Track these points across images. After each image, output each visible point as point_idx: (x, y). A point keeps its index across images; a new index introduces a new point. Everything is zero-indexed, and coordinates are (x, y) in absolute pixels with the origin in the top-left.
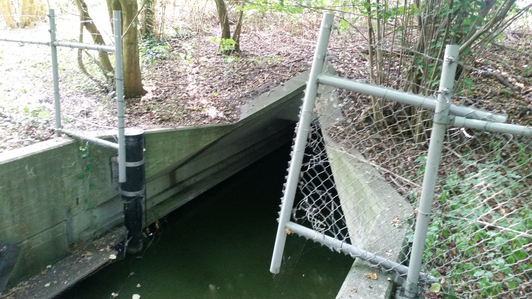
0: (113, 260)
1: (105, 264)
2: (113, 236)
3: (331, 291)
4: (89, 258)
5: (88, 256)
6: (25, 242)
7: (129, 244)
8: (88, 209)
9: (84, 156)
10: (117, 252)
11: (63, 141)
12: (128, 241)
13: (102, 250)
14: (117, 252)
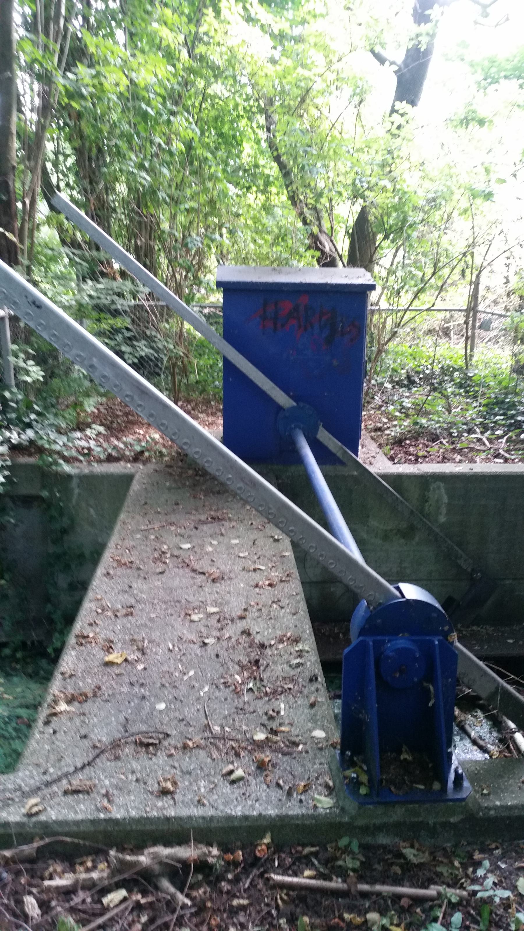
6: (507, 582)
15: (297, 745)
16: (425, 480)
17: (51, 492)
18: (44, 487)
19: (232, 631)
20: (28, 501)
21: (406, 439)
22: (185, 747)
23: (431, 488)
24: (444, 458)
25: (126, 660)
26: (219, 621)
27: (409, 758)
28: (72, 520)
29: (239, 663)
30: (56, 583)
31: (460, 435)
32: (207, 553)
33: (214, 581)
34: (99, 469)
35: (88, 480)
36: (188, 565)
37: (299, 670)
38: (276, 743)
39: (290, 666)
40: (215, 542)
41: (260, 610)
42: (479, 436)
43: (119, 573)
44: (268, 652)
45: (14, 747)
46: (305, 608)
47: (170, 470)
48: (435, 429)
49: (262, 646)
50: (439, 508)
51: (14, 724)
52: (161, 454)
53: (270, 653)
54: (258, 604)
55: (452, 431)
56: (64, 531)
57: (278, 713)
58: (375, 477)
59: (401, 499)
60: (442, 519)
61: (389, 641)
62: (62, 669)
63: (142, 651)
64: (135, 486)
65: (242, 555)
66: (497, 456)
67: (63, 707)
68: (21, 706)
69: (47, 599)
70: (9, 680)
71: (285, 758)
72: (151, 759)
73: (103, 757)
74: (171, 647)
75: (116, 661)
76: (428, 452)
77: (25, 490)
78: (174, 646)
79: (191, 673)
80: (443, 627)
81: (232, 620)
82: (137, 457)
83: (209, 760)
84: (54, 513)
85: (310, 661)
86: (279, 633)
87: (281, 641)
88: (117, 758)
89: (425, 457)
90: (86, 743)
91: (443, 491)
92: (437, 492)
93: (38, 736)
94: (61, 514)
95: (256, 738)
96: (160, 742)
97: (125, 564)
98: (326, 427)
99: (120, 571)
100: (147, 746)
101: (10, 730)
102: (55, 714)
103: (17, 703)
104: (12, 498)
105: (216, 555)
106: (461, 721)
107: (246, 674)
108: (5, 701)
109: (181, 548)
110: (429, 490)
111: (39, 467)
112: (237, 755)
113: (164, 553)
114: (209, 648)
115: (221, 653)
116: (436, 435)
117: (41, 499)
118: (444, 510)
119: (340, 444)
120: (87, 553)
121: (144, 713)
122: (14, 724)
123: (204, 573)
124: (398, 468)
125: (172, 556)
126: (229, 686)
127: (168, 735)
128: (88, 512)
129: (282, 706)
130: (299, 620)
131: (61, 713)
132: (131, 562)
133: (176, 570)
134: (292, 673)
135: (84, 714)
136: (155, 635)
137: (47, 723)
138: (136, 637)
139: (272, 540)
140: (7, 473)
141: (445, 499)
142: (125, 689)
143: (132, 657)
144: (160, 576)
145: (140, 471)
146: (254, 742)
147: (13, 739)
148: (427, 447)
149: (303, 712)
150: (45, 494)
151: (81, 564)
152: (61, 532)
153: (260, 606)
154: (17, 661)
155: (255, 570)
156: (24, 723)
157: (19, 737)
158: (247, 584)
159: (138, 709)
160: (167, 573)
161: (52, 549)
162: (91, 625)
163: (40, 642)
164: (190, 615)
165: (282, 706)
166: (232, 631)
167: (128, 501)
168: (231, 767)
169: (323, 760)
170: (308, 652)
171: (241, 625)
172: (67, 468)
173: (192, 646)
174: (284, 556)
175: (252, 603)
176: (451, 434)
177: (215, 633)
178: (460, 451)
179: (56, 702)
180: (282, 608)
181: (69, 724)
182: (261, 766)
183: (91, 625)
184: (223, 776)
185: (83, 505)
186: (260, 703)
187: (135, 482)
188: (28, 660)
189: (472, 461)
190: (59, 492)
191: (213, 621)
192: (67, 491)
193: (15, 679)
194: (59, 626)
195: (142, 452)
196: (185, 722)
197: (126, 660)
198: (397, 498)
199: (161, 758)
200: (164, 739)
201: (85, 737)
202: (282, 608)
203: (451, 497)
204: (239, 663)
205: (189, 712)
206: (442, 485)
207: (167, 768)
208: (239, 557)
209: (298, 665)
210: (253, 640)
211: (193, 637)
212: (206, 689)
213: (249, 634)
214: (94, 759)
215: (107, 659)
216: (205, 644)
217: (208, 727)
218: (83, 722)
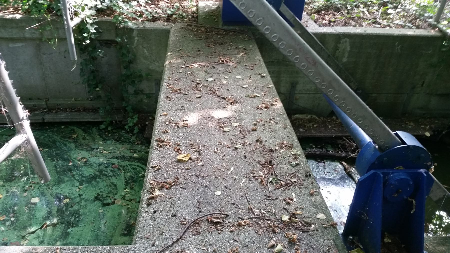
0: (427, 137)
1: (108, 41)
2: (437, 121)
3: (357, 238)
4: (410, 127)
5: (410, 125)
6: (374, 95)
7: (446, 133)
8: (427, 94)
9: (444, 49)
10: (433, 133)
11: (432, 32)
12: (446, 131)
13: (423, 126)
14: (433, 133)
15: (310, 225)
16: (339, 37)
17: (122, 38)
18: (117, 36)
19: (250, 139)
20: (108, 43)
21: (322, 10)
22: (240, 225)
23: (342, 42)
24: (346, 23)
25: (190, 159)
26: (241, 132)
27: (389, 241)
28: (135, 56)
29: (259, 162)
30: (127, 91)
31: (352, 9)
32: (223, 85)
33: (231, 103)
34: (149, 25)
35: (143, 32)
36: (214, 93)
37: (296, 168)
38: (296, 223)
39: (291, 165)
40: (227, 77)
41: (263, 125)
42: (362, 10)
43: (174, 97)
44: (275, 154)
45: (112, 181)
46: (290, 124)
47: (191, 28)
48: (337, 4)
49: (271, 151)
50: (344, 54)
51: (110, 168)
52: (183, 17)
53: (277, 156)
54: (261, 121)
55: (347, 6)
56: (131, 62)
57: (292, 200)
58: (310, 35)
59: (324, 48)
60: (345, 60)
61: (392, 173)
62: (152, 164)
63: (199, 152)
64: (172, 38)
65: (245, 86)
66: (375, 23)
67: (157, 192)
68: (113, 158)
69: (123, 99)
70: (105, 142)
71: (305, 235)
72: (220, 234)
73: (189, 233)
74: (216, 150)
75: (184, 159)
76: (336, 18)
77: (106, 37)
78: (217, 149)
79: (232, 169)
80: (427, 163)
81: (249, 132)
82: (169, 19)
83: (257, 235)
84: (125, 52)
85: (302, 161)
86: (279, 141)
87: (281, 147)
88: (198, 233)
89: (335, 22)
90: (176, 221)
91: (348, 44)
92: (345, 44)
93: (144, 215)
94: (129, 52)
95: (283, 219)
96: (223, 221)
97: (176, 91)
98: (286, 4)
99: (174, 95)
100: (216, 223)
101: (109, 171)
102: (153, 198)
103: (111, 156)
104: (99, 41)
105: (229, 86)
106: (350, 172)
107: (266, 171)
108: (104, 155)
109: (207, 81)
110: (340, 43)
111: (114, 23)
112: (274, 232)
113: (198, 84)
114: (239, 151)
115: (247, 154)
116: (338, 8)
117: (117, 43)
118: (346, 55)
119: (292, 14)
120: (144, 75)
121: (209, 197)
122: (110, 168)
123: (224, 98)
124: (323, 29)
125: (203, 86)
126: (257, 179)
127: (227, 216)
128: (143, 52)
129: (293, 194)
130: (288, 132)
131: (156, 197)
132: (180, 90)
133: (207, 95)
134: (294, 170)
135: (171, 198)
136: (204, 141)
137: (149, 205)
138: (192, 142)
139: (260, 76)
140: (96, 26)
141: (348, 48)
142: (194, 179)
143: (194, 156)
144: (199, 99)
145: (174, 28)
146: (282, 222)
147: (111, 177)
148: (335, 15)
149: (307, 199)
150: (119, 40)
151: (141, 81)
152: (129, 63)
153: (263, 122)
154: (109, 132)
155: (254, 97)
156: (116, 167)
157: (114, 176)
158: (252, 106)
159: (204, 194)
160: (202, 98)
161: (124, 72)
162: (164, 132)
163: (121, 122)
164: (222, 127)
165: (293, 194)
166: (250, 139)
167: (170, 48)
168: (273, 242)
169: (328, 237)
170: (300, 155)
171: (255, 135)
172: (130, 24)
173: (228, 149)
174: (270, 88)
175: (258, 120)
176: (346, 8)
177: (240, 141)
178: (353, 19)
179: (152, 188)
180: (277, 123)
181: (162, 205)
182: (292, 242)
183: (164, 132)
184: (268, 248)
185: (141, 47)
186: (279, 192)
187: (171, 35)
188: (114, 131)
189: (361, 25)
190: (126, 39)
191: (237, 132)
192: (131, 38)
193: (109, 142)
194: (131, 114)
195: (172, 15)
196: (235, 206)
197: (190, 159)
198: (322, 48)
199: (226, 234)
200: (225, 218)
201: (175, 216)
202: (277, 123)
203: (352, 47)
204: (259, 162)
205: (236, 197)
206: (348, 40)
207: (232, 241)
208: (243, 87)
209: (297, 165)
210: (264, 146)
211: (227, 143)
212: (243, 181)
213: (261, 142)
214: (183, 234)
215: (179, 158)
216: (236, 149)
217: (250, 210)
218: (172, 204)
